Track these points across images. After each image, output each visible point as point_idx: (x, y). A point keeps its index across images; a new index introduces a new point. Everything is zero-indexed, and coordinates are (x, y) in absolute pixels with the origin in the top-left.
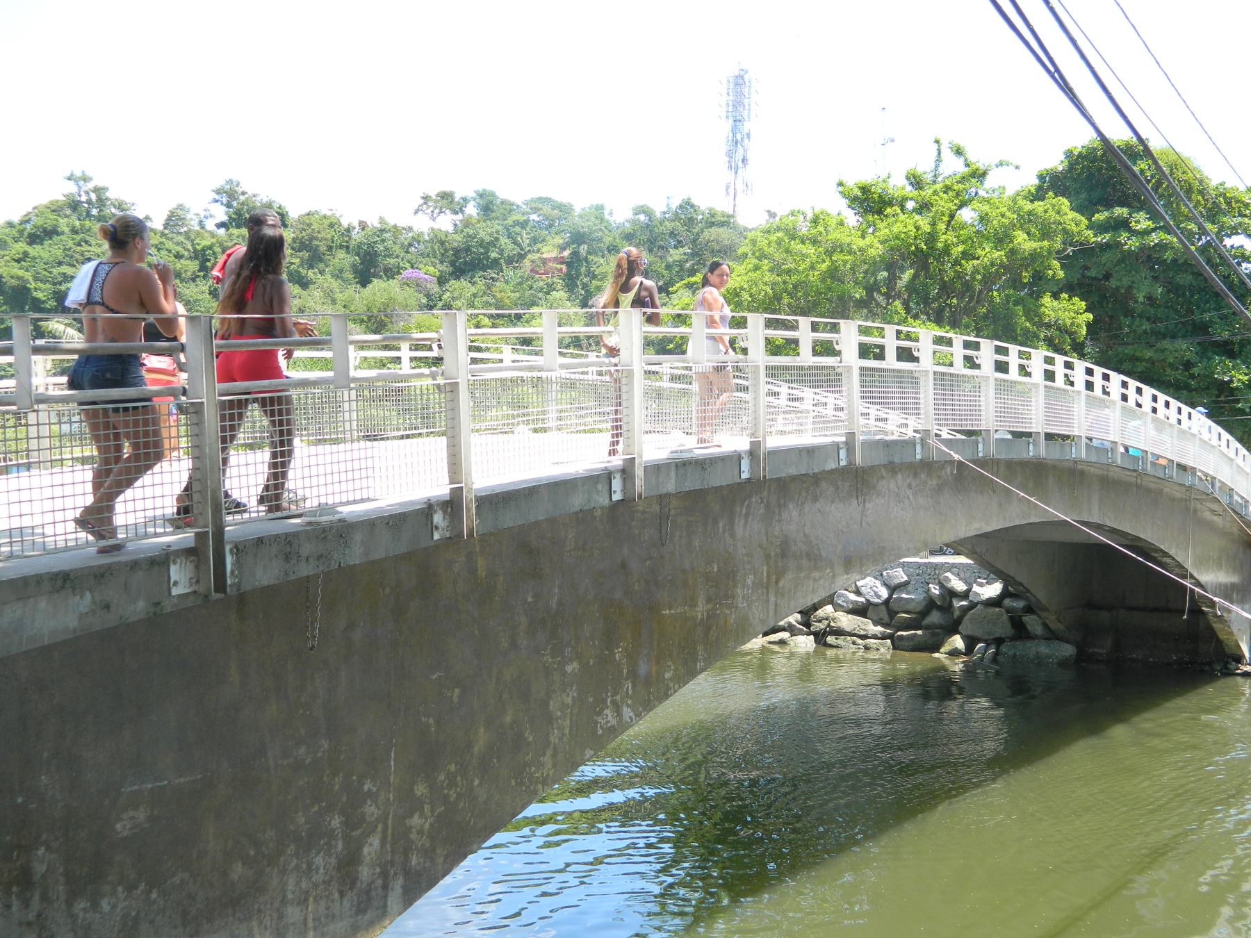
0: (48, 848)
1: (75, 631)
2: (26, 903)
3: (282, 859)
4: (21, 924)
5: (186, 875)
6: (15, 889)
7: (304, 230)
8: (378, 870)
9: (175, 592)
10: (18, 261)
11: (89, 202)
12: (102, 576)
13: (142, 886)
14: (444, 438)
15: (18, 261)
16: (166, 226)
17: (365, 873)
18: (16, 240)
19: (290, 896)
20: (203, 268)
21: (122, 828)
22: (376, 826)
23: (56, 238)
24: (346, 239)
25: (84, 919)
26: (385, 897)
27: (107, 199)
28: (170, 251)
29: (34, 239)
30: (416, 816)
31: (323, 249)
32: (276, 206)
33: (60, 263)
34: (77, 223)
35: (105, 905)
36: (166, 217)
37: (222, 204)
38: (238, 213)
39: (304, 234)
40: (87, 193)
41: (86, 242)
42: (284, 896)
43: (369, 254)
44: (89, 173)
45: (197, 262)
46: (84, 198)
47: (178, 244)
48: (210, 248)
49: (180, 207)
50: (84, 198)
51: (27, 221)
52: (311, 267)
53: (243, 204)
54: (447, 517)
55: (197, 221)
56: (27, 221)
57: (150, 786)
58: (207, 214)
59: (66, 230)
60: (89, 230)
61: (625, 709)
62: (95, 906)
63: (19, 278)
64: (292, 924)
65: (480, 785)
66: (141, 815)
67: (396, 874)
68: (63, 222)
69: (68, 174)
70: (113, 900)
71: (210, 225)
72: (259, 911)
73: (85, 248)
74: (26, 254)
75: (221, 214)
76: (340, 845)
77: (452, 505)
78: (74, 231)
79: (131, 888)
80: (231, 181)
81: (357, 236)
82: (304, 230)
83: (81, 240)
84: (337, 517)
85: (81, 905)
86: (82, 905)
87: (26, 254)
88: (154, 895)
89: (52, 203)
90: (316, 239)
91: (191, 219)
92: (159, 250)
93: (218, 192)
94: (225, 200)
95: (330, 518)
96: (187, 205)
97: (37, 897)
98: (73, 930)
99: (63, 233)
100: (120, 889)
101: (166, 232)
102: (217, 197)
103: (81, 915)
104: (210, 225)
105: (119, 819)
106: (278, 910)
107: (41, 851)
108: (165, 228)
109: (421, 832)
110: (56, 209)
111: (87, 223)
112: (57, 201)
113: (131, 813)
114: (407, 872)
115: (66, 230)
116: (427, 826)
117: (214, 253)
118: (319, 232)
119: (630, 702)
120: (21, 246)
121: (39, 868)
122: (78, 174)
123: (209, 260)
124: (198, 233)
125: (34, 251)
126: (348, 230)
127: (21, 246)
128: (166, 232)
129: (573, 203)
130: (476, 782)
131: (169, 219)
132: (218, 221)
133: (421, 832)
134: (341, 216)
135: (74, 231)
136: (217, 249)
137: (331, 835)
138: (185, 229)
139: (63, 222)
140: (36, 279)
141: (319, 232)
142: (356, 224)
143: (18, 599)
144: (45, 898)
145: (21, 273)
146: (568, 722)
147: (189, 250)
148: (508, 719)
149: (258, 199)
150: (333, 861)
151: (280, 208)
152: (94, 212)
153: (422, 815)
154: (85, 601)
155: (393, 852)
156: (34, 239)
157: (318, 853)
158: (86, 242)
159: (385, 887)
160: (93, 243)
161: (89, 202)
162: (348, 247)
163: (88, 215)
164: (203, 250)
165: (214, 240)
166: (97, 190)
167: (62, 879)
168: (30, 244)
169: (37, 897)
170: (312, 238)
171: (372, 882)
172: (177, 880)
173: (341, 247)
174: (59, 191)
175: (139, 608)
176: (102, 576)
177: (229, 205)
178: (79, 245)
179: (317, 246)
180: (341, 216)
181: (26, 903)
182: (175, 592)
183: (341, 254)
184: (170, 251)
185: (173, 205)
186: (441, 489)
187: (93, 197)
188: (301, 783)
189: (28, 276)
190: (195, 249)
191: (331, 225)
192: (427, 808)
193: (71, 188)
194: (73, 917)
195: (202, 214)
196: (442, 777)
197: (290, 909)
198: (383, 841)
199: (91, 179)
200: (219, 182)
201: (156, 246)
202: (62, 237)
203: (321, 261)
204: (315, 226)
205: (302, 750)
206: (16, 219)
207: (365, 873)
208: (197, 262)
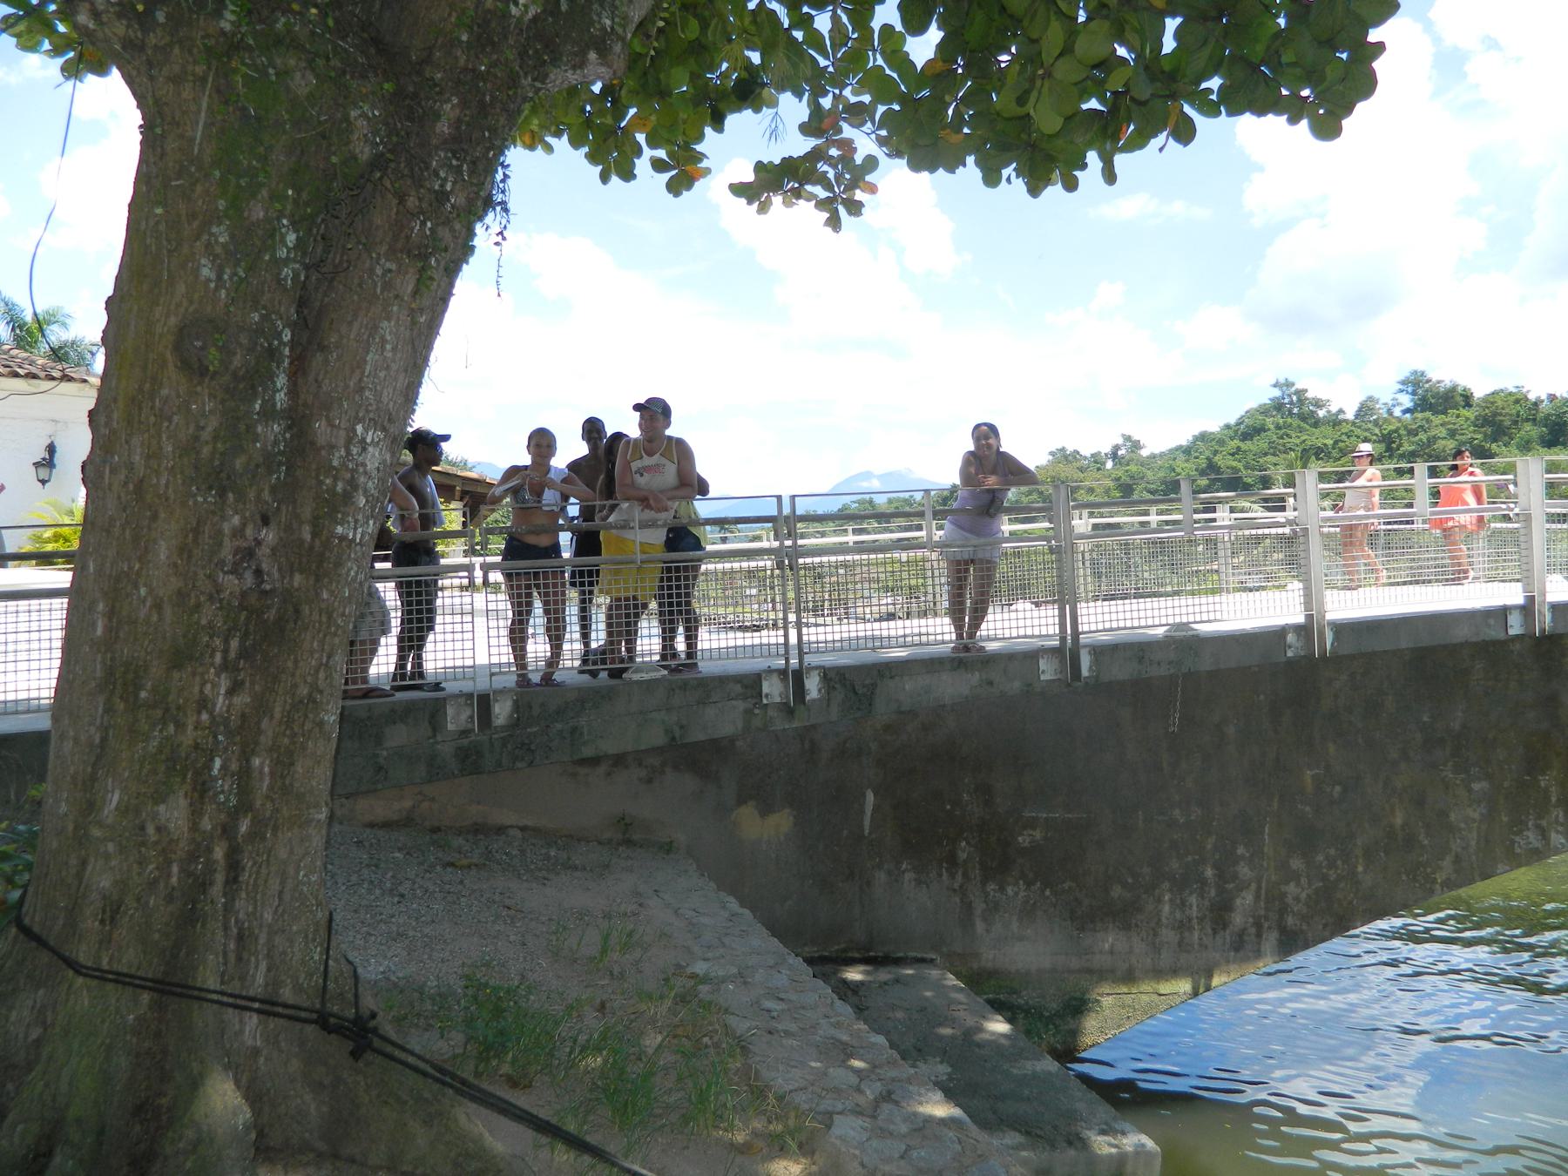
0: (968, 843)
1: (967, 697)
2: (952, 876)
3: (1157, 891)
4: (948, 889)
5: (1074, 885)
6: (945, 865)
7: (1488, 408)
8: (1251, 920)
9: (1042, 678)
10: (1233, 455)
11: (1291, 403)
12: (987, 662)
13: (1038, 884)
14: (1519, 584)
15: (1233, 455)
16: (1357, 416)
17: (1238, 920)
18: (1232, 439)
19: (1164, 920)
20: (1389, 449)
21: (1023, 840)
22: (1249, 885)
23: (1263, 434)
24: (1534, 412)
25: (994, 896)
26: (1259, 944)
27: (1306, 399)
28: (1358, 437)
29: (1246, 436)
30: (1292, 885)
31: (1507, 423)
32: (1460, 389)
33: (1266, 454)
34: (1281, 421)
35: (1010, 890)
36: (1356, 409)
37: (1407, 393)
38: (1424, 399)
39: (1487, 411)
40: (1289, 396)
41: (1287, 435)
42: (1160, 920)
43: (1558, 424)
44: (1291, 379)
45: (1384, 445)
46: (1286, 401)
47: (1366, 430)
48: (1396, 431)
49: (1370, 399)
50: (1286, 401)
51: (1241, 423)
52: (1495, 440)
53: (1427, 391)
54: (1301, 638)
55: (1385, 410)
56: (1241, 423)
57: (1045, 815)
58: (1395, 402)
59: (1272, 427)
60: (1291, 425)
61: (1553, 835)
62: (1002, 889)
63: (1233, 468)
64: (1167, 943)
65: (1365, 871)
66: (1038, 834)
67: (1269, 928)
68: (1269, 420)
69: (1274, 382)
70: (1016, 889)
71: (1397, 412)
72: (1137, 926)
73: (1287, 440)
74: (1239, 448)
75: (1406, 401)
76: (1213, 893)
77: (1304, 630)
78: (1278, 427)
79: (1029, 884)
80: (1415, 372)
81: (1545, 407)
82: (1488, 408)
83: (1284, 434)
84: (1190, 633)
85: (991, 887)
86: (992, 887)
87: (1239, 448)
88: (1048, 893)
89: (1260, 406)
90: (1501, 414)
91: (1379, 409)
92: (1349, 437)
93: (1403, 383)
94: (1410, 389)
95: (1184, 633)
96: (1376, 396)
97: (960, 873)
98: (985, 902)
99: (1269, 429)
100: (1021, 882)
101: (1357, 421)
102: (1401, 387)
103: (992, 893)
104: (1397, 412)
105: (1021, 834)
106: (1153, 929)
107: (963, 844)
108: (1356, 418)
109: (1297, 899)
110: (1264, 411)
111: (1289, 420)
112: (1265, 405)
113: (1031, 832)
114: (1283, 930)
115: (1272, 427)
116: (1304, 895)
117: (1399, 435)
118: (1503, 409)
119: (1560, 829)
120: (1236, 443)
121: (963, 856)
122: (1282, 380)
123: (1394, 442)
124: (1385, 420)
125: (1244, 446)
126: (1536, 404)
127: (1236, 443)
128: (1357, 421)
129: (1420, 368)
130: (1360, 869)
131: (1360, 410)
132: (1404, 408)
133: (1297, 899)
134: (1528, 392)
135: (1278, 427)
136: (1402, 432)
137: (1203, 882)
138: (1375, 417)
139: (1269, 420)
140: (1246, 468)
141: (1503, 409)
142: (1544, 397)
143: (928, 672)
144: (965, 875)
145: (1234, 464)
146: (1475, 834)
147: (1376, 435)
148: (1399, 820)
149: (1442, 385)
150: (1207, 903)
151: (1464, 390)
152: (1295, 410)
153: (1298, 884)
154: (975, 677)
155: (1267, 909)
156: (1246, 436)
157: (1191, 893)
158: (1287, 435)
159: (1259, 935)
160: (1294, 435)
161: (1291, 403)
162: (1534, 420)
163: (1291, 413)
164: (1390, 433)
165: (1400, 425)
166: (1298, 392)
167: (977, 866)
168: (1243, 440)
169: (960, 873)
170: (1495, 414)
171: (1245, 929)
172: (1066, 886)
173: (1527, 420)
174: (1266, 395)
175: (1015, 686)
176: (987, 662)
177: (1414, 393)
178: (1282, 438)
179: (1502, 421)
180: (1528, 392)
181: (952, 876)
182: (1042, 678)
183: (1528, 427)
184: (1358, 437)
185: (1363, 398)
186: (1300, 619)
187: (1295, 398)
188: (1175, 837)
189: (1240, 466)
190: (1383, 434)
191: (1517, 401)
192: (1304, 881)
193: (1277, 393)
194: (987, 895)
195: (1391, 403)
196: (1320, 858)
197: (1164, 931)
198: (1257, 897)
199: (1293, 384)
200: (1404, 373)
201: (1346, 434)
202: (1269, 433)
203: (1505, 435)
204: (1500, 403)
205: (1177, 812)
206: (1232, 421)
207: (1238, 919)
208: (1384, 445)
